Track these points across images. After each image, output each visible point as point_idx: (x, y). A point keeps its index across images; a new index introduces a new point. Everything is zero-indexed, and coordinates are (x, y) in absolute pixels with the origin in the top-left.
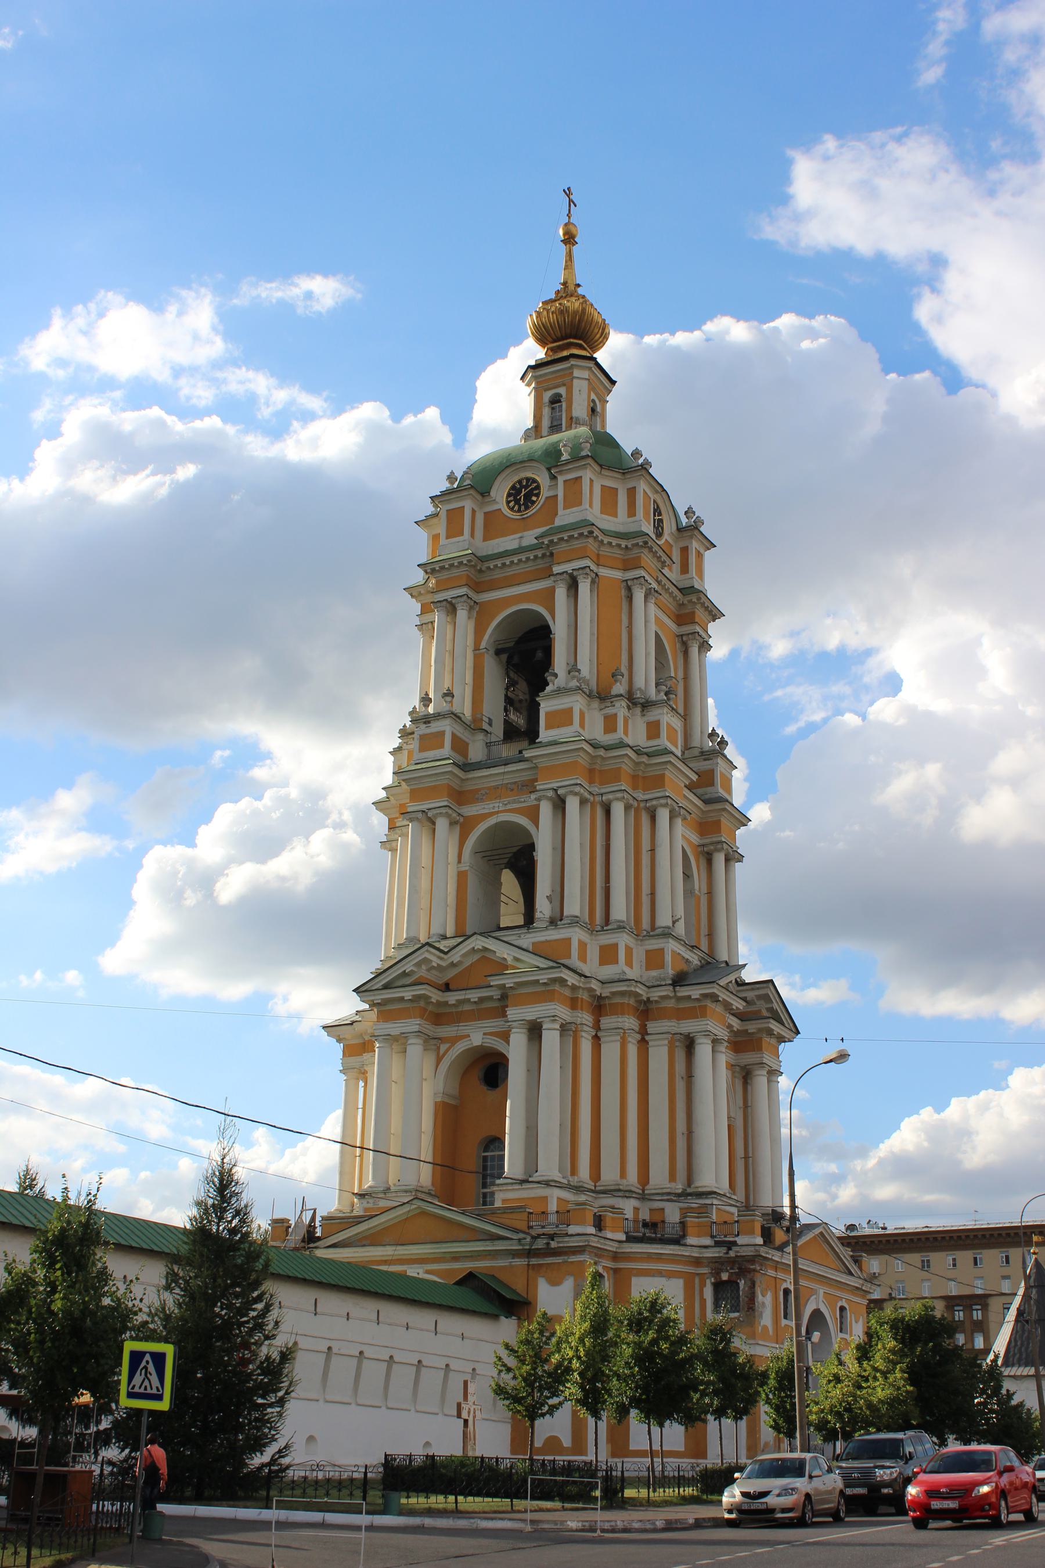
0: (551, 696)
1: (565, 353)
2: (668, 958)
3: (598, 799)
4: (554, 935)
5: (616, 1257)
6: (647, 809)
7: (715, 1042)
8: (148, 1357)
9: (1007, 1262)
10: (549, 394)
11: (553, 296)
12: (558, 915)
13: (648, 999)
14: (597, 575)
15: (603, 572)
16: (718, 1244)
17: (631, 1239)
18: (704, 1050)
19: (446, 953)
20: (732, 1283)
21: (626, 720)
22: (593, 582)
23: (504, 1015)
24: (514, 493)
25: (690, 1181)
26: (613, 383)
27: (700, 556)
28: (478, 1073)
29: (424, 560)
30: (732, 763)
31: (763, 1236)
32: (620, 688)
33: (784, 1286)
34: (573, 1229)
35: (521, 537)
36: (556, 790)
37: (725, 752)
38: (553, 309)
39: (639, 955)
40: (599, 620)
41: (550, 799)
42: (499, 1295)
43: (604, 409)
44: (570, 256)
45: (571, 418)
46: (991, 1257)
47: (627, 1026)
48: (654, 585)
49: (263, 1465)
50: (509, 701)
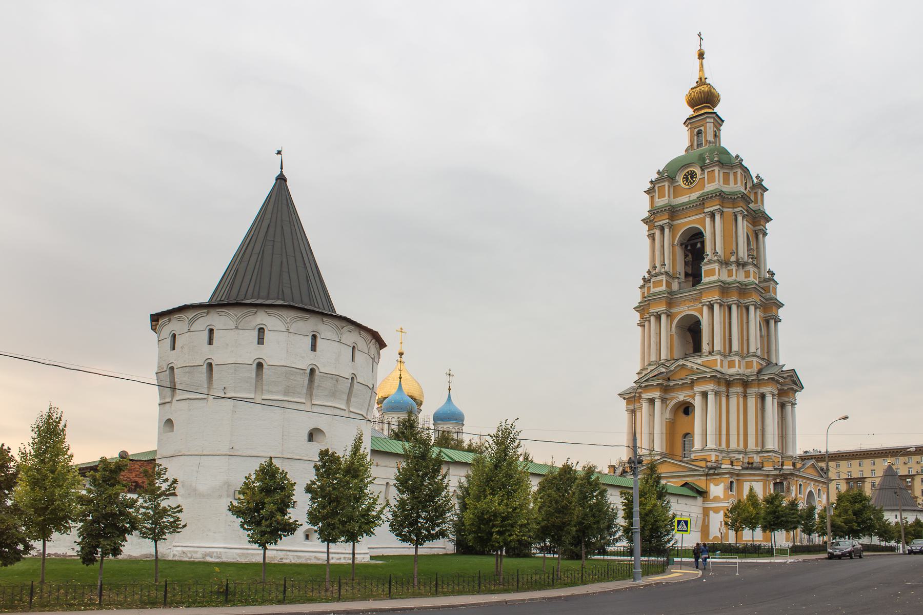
0: (706, 264)
1: (703, 112)
2: (755, 364)
3: (726, 304)
4: (710, 358)
5: (738, 475)
6: (746, 307)
7: (773, 395)
8: (683, 521)
9: (874, 464)
10: (697, 130)
11: (695, 85)
12: (711, 350)
13: (747, 380)
14: (723, 211)
15: (725, 210)
16: (776, 469)
17: (743, 469)
18: (769, 399)
19: (668, 367)
20: (781, 483)
21: (737, 270)
22: (721, 214)
23: (692, 389)
24: (686, 178)
25: (763, 446)
26: (723, 121)
27: (762, 195)
28: (682, 410)
29: (649, 210)
30: (776, 282)
31: (793, 466)
32: (733, 259)
33: (800, 483)
34: (723, 466)
35: (690, 196)
36: (710, 302)
37: (774, 278)
38: (696, 91)
39: (743, 363)
40: (724, 230)
41: (707, 305)
42: (697, 490)
43: (719, 133)
44: (702, 65)
45: (707, 141)
46: (867, 463)
47: (738, 391)
48: (746, 213)
49: (670, 547)
50: (686, 263)
